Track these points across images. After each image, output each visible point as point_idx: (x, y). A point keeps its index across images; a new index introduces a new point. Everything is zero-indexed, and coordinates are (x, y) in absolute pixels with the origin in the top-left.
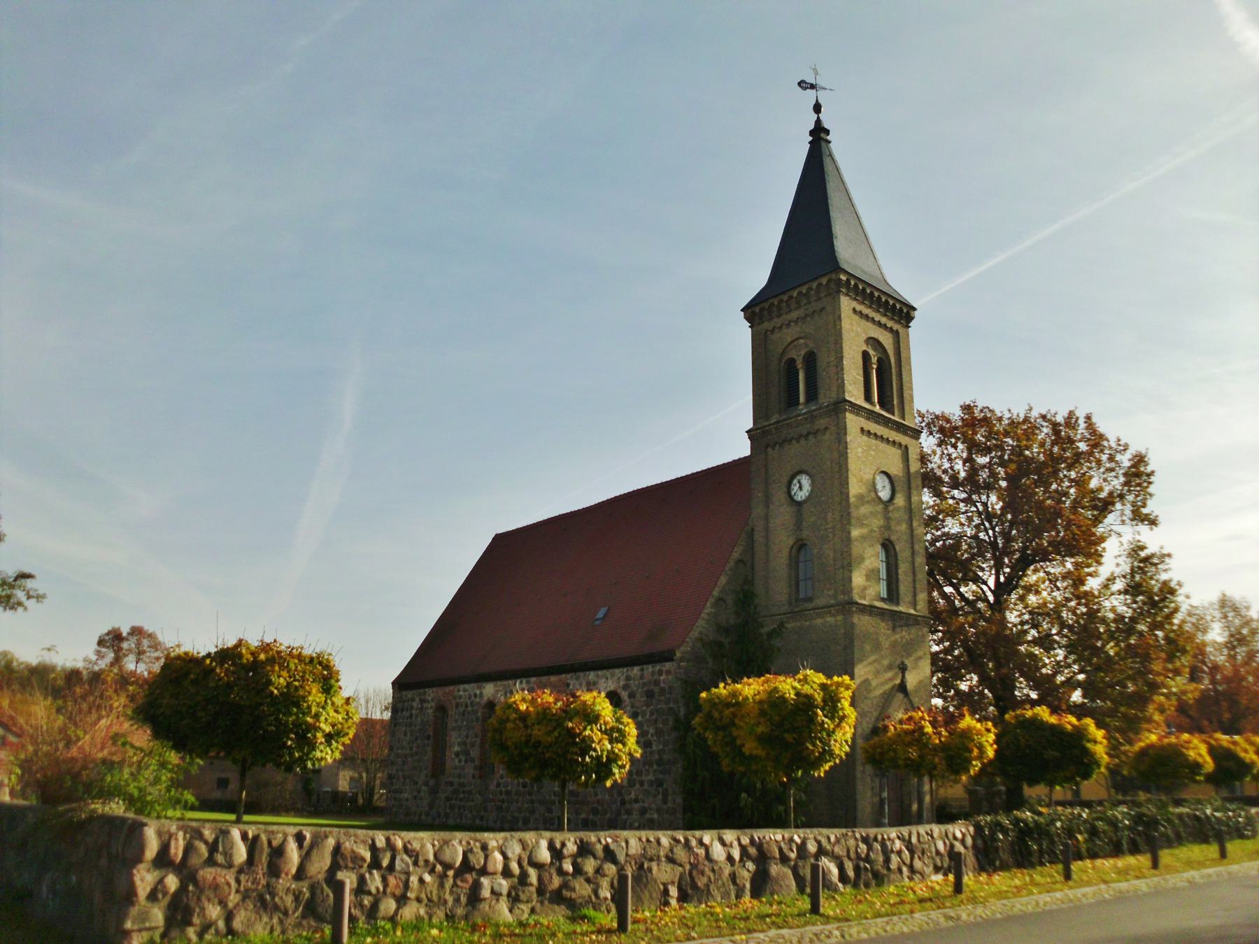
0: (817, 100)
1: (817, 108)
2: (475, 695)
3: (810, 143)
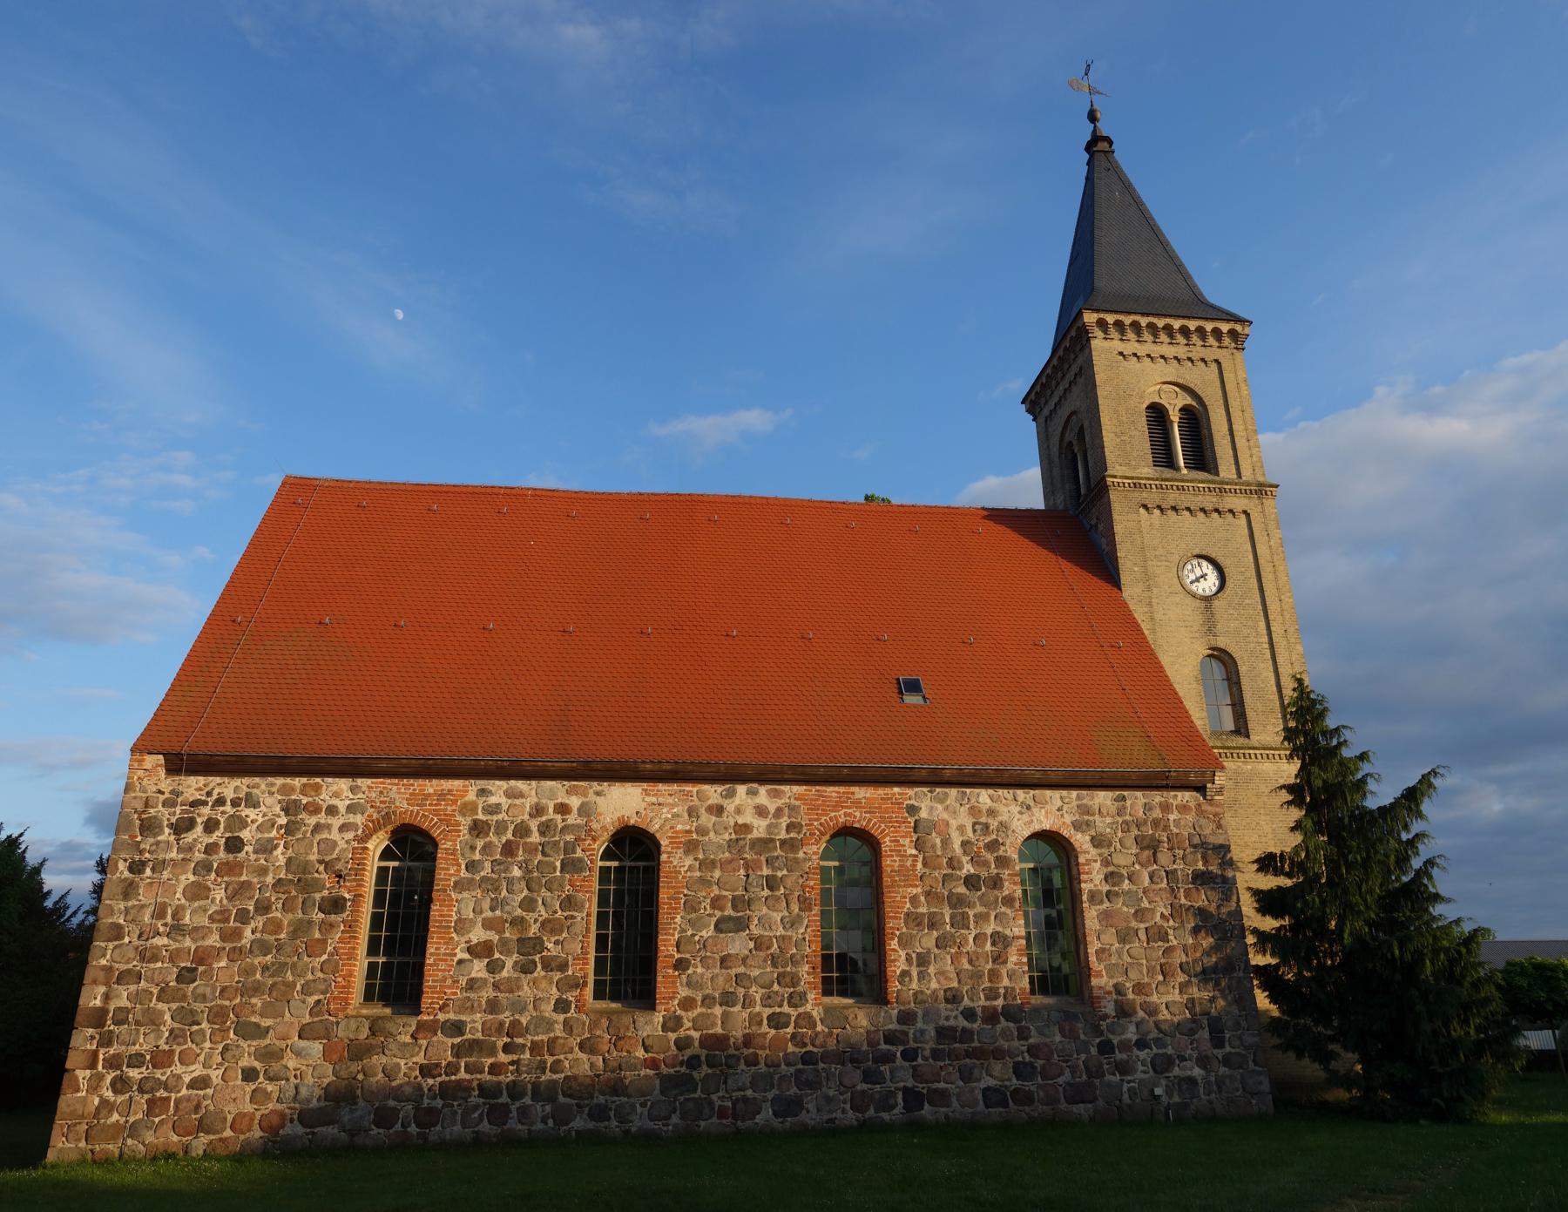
1: (1092, 117)
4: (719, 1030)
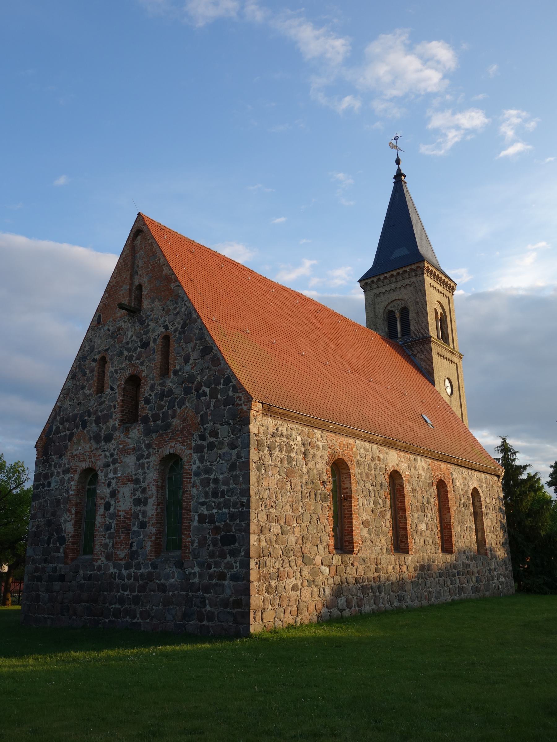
0: (398, 156)
1: (398, 162)
3: (394, 183)
4: (422, 563)
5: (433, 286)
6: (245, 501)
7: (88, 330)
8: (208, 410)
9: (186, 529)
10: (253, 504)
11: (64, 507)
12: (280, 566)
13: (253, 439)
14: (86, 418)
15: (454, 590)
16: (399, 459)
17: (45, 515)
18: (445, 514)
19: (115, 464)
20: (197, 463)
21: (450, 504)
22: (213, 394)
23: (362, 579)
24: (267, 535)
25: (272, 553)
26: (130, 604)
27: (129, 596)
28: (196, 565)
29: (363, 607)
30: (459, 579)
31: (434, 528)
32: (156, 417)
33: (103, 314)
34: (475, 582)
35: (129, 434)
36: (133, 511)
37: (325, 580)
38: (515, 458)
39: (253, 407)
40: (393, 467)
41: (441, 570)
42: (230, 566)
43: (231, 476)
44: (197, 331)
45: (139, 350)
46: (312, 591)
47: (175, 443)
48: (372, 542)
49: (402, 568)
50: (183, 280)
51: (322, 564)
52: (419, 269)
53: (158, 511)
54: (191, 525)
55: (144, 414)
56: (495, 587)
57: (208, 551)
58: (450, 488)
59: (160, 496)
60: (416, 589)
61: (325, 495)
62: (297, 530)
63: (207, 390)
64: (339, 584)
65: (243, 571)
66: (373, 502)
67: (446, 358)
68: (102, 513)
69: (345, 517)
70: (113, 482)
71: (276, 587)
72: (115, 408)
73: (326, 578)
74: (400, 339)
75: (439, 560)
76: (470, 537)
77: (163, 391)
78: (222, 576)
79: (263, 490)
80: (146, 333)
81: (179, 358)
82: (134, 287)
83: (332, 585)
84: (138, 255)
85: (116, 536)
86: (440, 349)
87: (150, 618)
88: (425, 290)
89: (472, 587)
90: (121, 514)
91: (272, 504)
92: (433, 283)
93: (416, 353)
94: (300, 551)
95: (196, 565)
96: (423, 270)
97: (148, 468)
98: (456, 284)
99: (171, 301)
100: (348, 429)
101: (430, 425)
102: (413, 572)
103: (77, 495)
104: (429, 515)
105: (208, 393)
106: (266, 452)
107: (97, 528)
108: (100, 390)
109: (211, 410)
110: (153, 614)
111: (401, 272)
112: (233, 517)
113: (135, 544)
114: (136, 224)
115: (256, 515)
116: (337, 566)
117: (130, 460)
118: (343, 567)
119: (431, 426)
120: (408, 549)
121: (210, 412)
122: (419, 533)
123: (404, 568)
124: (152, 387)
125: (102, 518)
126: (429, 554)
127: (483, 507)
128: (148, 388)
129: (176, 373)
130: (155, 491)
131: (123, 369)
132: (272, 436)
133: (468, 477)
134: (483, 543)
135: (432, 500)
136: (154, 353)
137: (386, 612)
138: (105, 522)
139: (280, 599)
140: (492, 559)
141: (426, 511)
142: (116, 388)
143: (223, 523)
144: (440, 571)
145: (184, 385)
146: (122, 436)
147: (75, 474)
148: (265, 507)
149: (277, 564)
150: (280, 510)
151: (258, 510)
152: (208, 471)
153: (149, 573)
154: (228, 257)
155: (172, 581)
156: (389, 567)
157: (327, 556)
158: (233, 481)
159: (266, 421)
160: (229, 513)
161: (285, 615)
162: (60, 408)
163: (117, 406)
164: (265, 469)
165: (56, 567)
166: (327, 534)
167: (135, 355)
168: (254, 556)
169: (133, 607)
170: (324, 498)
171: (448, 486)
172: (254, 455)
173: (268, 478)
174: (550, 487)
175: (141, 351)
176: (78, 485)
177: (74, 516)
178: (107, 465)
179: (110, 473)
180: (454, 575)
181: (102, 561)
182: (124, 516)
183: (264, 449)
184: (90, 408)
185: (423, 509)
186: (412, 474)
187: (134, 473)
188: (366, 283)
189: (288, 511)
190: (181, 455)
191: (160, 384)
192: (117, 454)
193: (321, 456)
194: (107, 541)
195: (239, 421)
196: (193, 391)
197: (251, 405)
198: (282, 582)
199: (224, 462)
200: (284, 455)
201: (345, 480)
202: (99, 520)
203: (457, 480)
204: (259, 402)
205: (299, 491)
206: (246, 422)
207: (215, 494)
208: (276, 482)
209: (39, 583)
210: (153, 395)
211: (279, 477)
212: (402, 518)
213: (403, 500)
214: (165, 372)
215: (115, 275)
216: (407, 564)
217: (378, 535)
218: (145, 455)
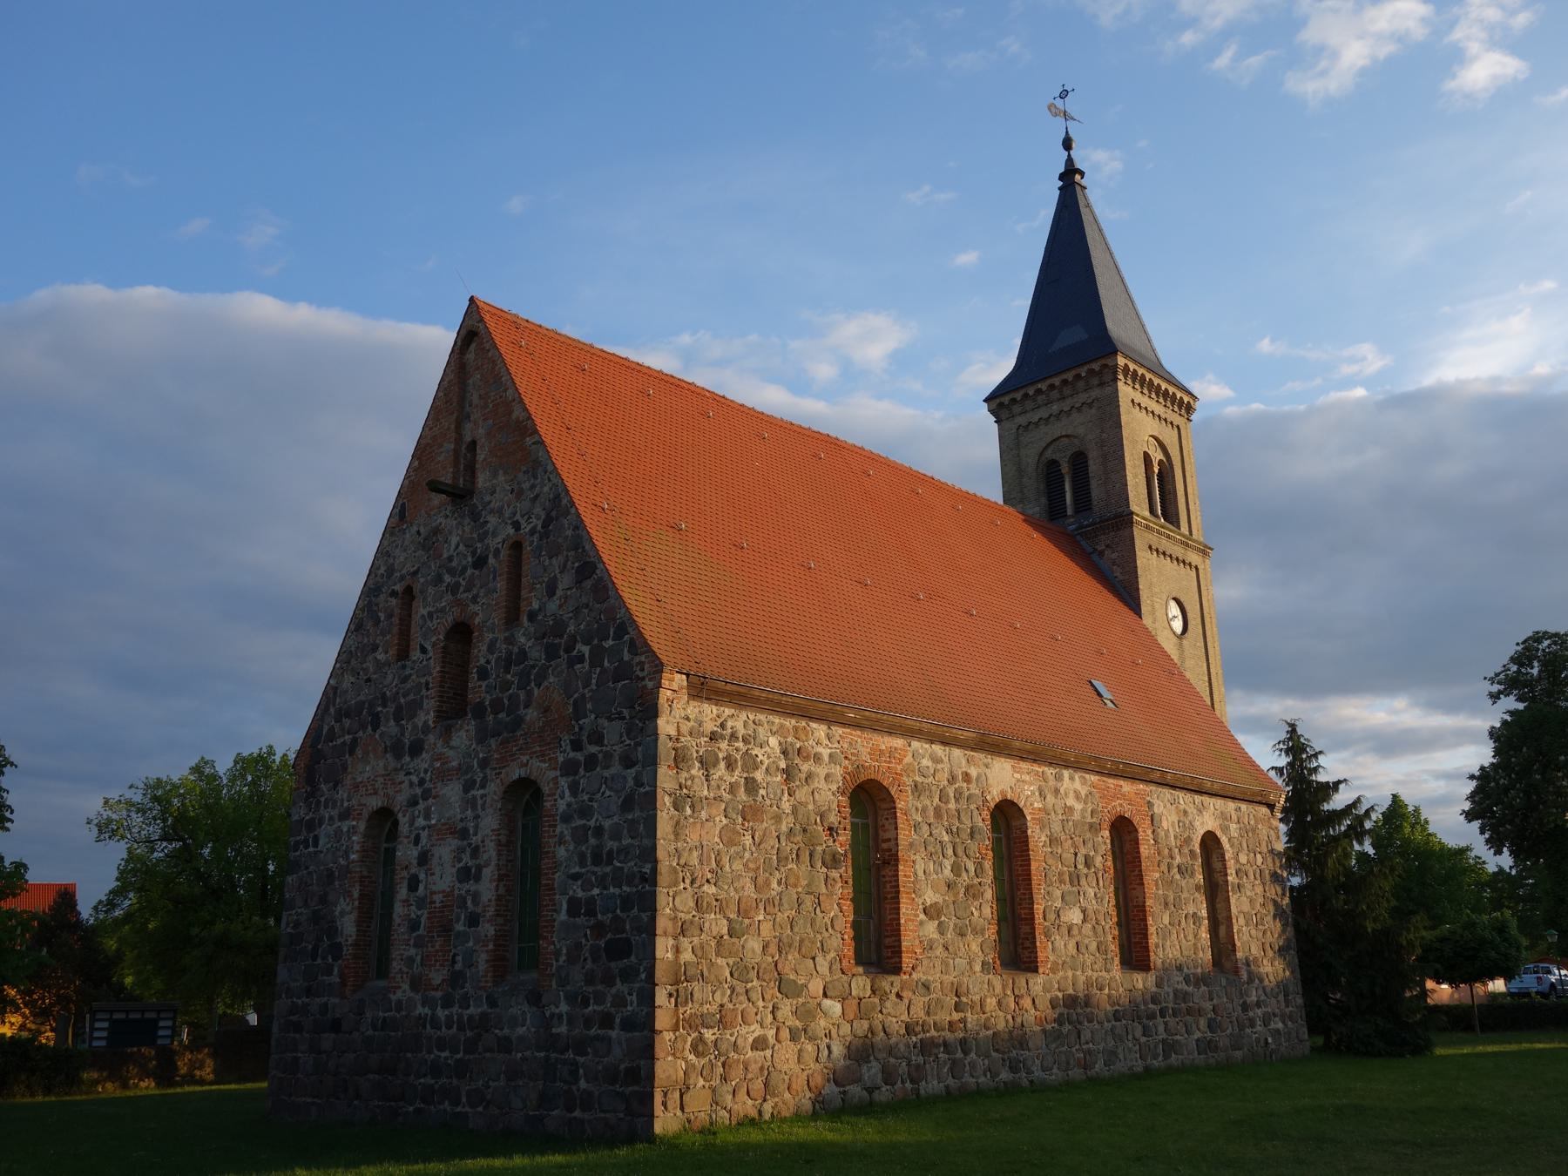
0: (1067, 132)
1: (1067, 144)
2: (967, 777)
3: (1059, 189)
4: (1071, 991)
5: (1139, 405)
6: (648, 871)
7: (383, 535)
8: (586, 691)
9: (546, 927)
10: (664, 877)
11: (340, 885)
12: (726, 1000)
13: (665, 748)
14: (380, 709)
15: (1152, 1046)
16: (1017, 776)
17: (309, 900)
18: (1134, 889)
19: (426, 799)
20: (566, 796)
21: (1143, 868)
22: (596, 660)
23: (923, 1026)
24: (696, 940)
25: (706, 973)
26: (451, 1077)
27: (449, 1061)
28: (562, 998)
29: (924, 1083)
30: (1166, 1024)
31: (1101, 918)
32: (497, 706)
33: (408, 501)
34: (1206, 1029)
35: (450, 739)
36: (456, 892)
37: (831, 1027)
38: (1319, 766)
39: (665, 683)
40: (1002, 792)
41: (1119, 1005)
42: (620, 1002)
43: (625, 822)
44: (569, 533)
45: (469, 572)
46: (800, 1051)
47: (528, 757)
48: (947, 949)
49: (1021, 1002)
50: (547, 431)
51: (825, 995)
52: (1106, 370)
53: (499, 893)
54: (554, 921)
55: (478, 700)
56: (1258, 1040)
57: (584, 971)
58: (1145, 834)
59: (504, 862)
60: (1054, 1046)
61: (834, 856)
62: (766, 929)
63: (586, 650)
64: (866, 1037)
65: (642, 1011)
66: (949, 868)
67: (1171, 556)
68: (404, 897)
69: (886, 898)
70: (424, 835)
71: (716, 1043)
72: (428, 689)
73: (833, 1024)
74: (1072, 520)
75: (1113, 985)
76: (1195, 936)
77: (510, 653)
78: (607, 1021)
79: (688, 848)
80: (481, 540)
81: (538, 586)
82: (464, 446)
83: (849, 1039)
84: (471, 381)
85: (428, 942)
86: (1155, 539)
87: (484, 1104)
88: (1119, 415)
89: (1198, 1040)
90: (438, 898)
91: (709, 876)
92: (1138, 398)
93: (1104, 547)
94: (774, 968)
95: (562, 998)
96: (1115, 373)
97: (483, 806)
98: (1195, 398)
99: (524, 472)
100: (890, 718)
101: (1108, 702)
102: (1049, 1011)
103: (363, 861)
104: (1091, 892)
105: (587, 656)
106: (696, 771)
107: (396, 927)
108: (403, 654)
109: (591, 690)
110: (489, 1097)
111: (1057, 383)
112: (626, 903)
113: (459, 958)
114: (466, 319)
115: (671, 899)
116: (861, 999)
117: (452, 791)
118: (877, 1000)
119: (1110, 704)
120: (1037, 962)
121: (590, 694)
122: (1064, 930)
123: (1027, 1002)
124: (492, 647)
125: (404, 906)
126: (1090, 973)
127: (1229, 871)
128: (485, 648)
129: (532, 616)
130: (494, 853)
131: (442, 610)
132: (711, 739)
133: (1191, 810)
134: (1230, 947)
135: (1098, 861)
136: (494, 578)
137: (979, 1093)
138: (409, 915)
139: (724, 1067)
140: (1250, 980)
141: (1083, 882)
142: (429, 648)
143: (610, 915)
144: (1117, 1007)
145: (545, 641)
146: (440, 743)
147: (359, 819)
148: (692, 883)
149: (718, 996)
150: (726, 887)
151: (675, 889)
152: (585, 812)
153: (484, 1015)
154: (669, 373)
155: (521, 1030)
156: (988, 1000)
157: (837, 980)
158: (629, 831)
159: (697, 710)
160: (620, 895)
161: (737, 1099)
162: (335, 689)
163: (431, 685)
164: (693, 807)
165: (326, 1004)
166: (839, 935)
167: (464, 583)
168: (664, 980)
169: (455, 1081)
170: (833, 861)
171: (1140, 830)
172: (666, 778)
173: (699, 826)
174: (1470, 821)
175: (473, 574)
176: (364, 842)
177: (357, 903)
178: (413, 802)
179: (418, 817)
180: (1152, 1016)
181: (403, 992)
182: (442, 902)
183: (689, 768)
184: (385, 689)
185: (1075, 879)
186: (1050, 806)
187: (459, 817)
188: (1001, 405)
189: (746, 889)
190: (538, 781)
191: (506, 638)
192: (431, 780)
193: (827, 777)
194: (413, 951)
195: (640, 711)
196: (562, 653)
197: (661, 678)
198: (729, 1032)
199: (612, 794)
200: (737, 776)
201: (887, 823)
202: (399, 909)
203: (1164, 818)
204: (677, 672)
205: (773, 847)
206: (652, 712)
207: (597, 860)
208: (717, 832)
209: (297, 1036)
210: (493, 663)
211: (725, 821)
212: (1025, 899)
213: (1027, 861)
214: (512, 617)
215: (431, 423)
216: (1033, 994)
217: (962, 935)
218: (478, 780)
